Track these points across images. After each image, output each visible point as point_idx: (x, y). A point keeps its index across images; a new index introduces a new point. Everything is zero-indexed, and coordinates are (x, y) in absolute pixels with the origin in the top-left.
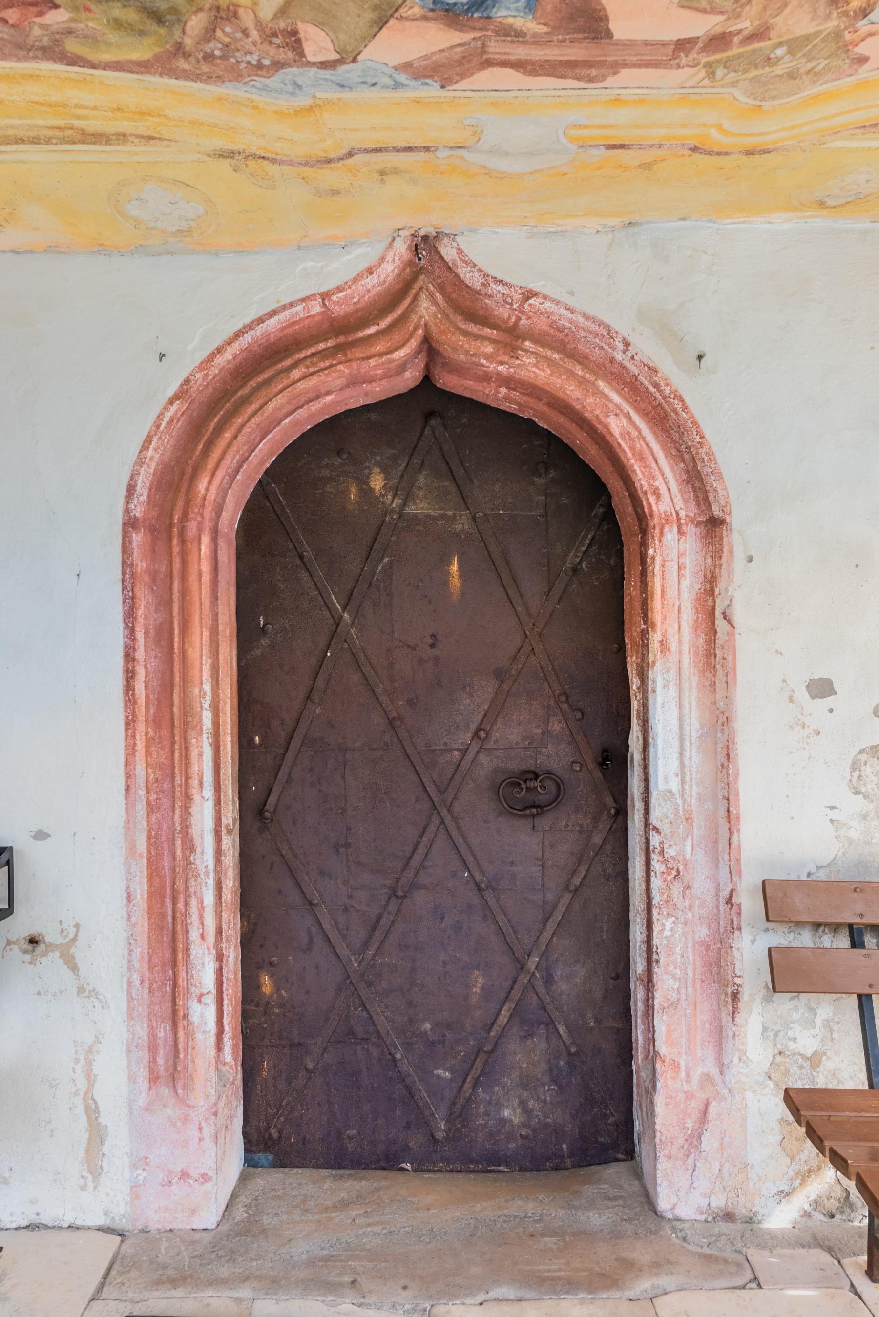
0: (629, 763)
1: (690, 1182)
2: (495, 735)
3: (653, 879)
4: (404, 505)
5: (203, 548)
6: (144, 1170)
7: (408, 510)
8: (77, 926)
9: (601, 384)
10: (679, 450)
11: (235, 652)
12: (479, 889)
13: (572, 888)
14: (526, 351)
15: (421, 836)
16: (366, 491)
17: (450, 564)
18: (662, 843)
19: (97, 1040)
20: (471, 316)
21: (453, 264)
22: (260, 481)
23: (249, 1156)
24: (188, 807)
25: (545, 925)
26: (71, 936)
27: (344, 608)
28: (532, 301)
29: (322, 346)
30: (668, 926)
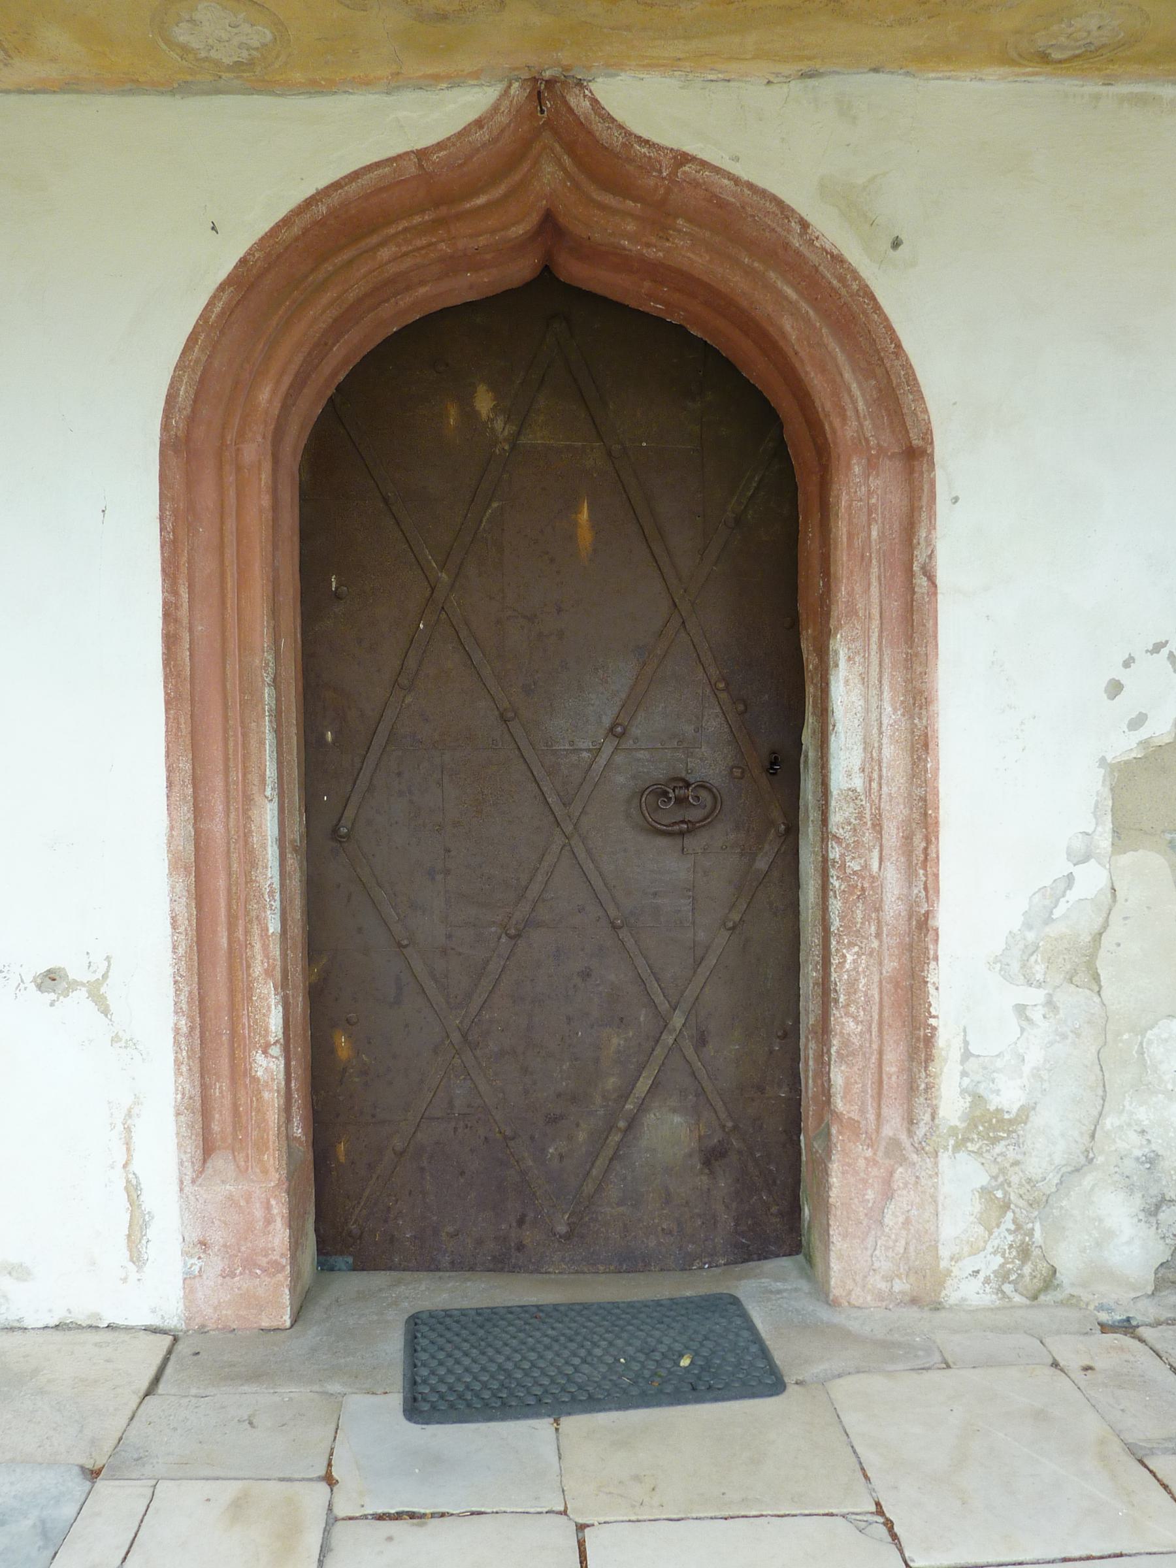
0: (802, 766)
1: (870, 1263)
2: (635, 731)
3: (832, 901)
4: (519, 433)
5: (263, 477)
6: (199, 1258)
7: (523, 440)
8: (108, 959)
9: (772, 275)
10: (869, 363)
11: (299, 621)
12: (615, 927)
13: (730, 924)
14: (679, 231)
15: (541, 860)
16: (469, 414)
17: (578, 512)
18: (842, 855)
19: (137, 1102)
20: (608, 185)
21: (586, 118)
22: (331, 400)
23: (323, 1258)
24: (248, 810)
25: (695, 972)
26: (102, 970)
27: (442, 567)
28: (686, 168)
29: (417, 219)
30: (850, 958)
